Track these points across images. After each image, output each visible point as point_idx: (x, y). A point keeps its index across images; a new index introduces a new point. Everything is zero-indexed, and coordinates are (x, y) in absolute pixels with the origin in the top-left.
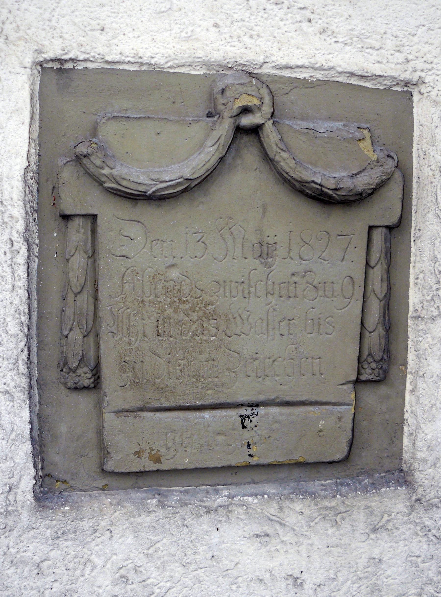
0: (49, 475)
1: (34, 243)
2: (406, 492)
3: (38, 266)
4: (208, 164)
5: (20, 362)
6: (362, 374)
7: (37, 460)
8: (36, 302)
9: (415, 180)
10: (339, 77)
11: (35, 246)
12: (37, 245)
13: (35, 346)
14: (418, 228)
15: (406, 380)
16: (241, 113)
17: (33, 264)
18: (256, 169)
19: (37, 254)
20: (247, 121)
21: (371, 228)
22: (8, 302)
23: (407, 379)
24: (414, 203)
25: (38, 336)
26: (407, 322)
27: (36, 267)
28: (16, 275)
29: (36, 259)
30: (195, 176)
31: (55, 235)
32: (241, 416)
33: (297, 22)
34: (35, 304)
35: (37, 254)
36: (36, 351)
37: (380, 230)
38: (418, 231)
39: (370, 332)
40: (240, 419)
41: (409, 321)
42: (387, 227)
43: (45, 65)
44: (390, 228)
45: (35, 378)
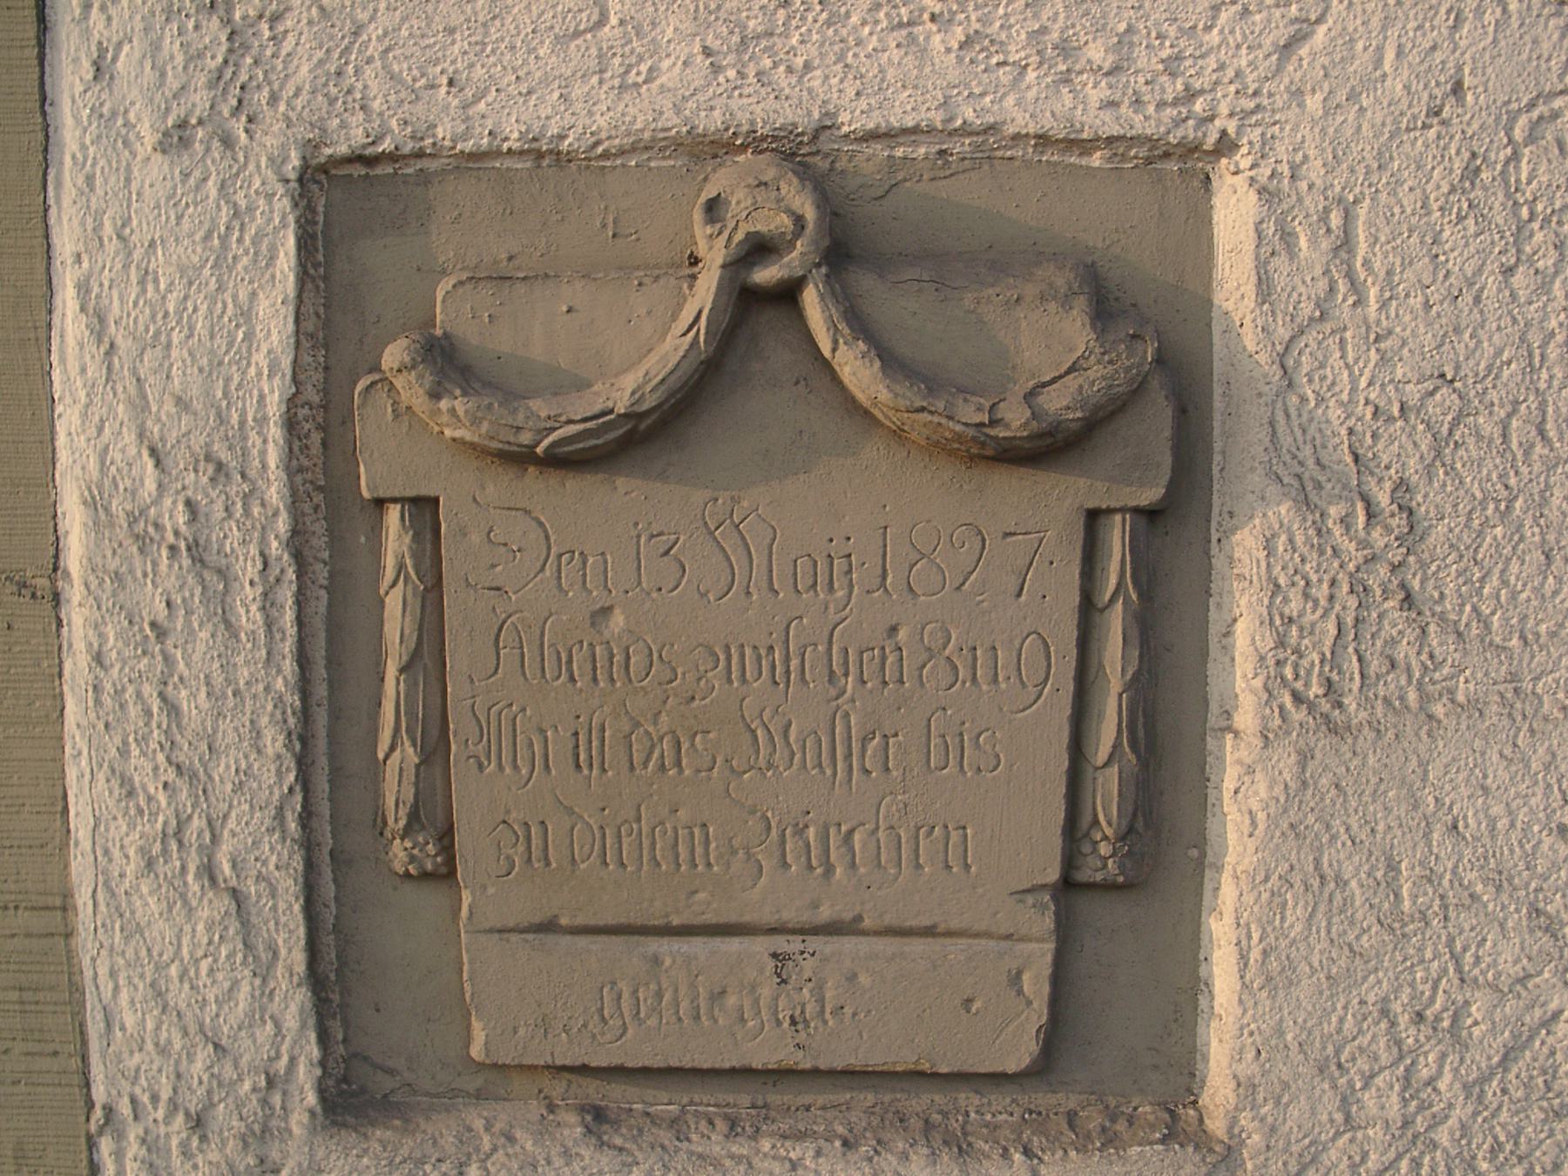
0: (355, 1055)
1: (315, 558)
2: (1198, 1158)
3: (330, 605)
4: (673, 378)
5: (289, 816)
6: (1078, 868)
7: (330, 1023)
8: (325, 685)
9: (1218, 391)
10: (1011, 148)
11: (319, 567)
12: (326, 564)
13: (325, 778)
14: (1226, 509)
15: (1202, 884)
16: (749, 254)
17: (313, 603)
18: (797, 383)
19: (325, 583)
20: (766, 274)
21: (1094, 517)
22: (261, 687)
23: (1206, 880)
24: (1217, 446)
25: (332, 757)
26: (1204, 740)
27: (323, 610)
28: (274, 629)
29: (323, 593)
30: (645, 407)
31: (363, 539)
32: (775, 955)
33: (901, 25)
34: (321, 691)
35: (325, 583)
36: (327, 789)
37: (1118, 518)
38: (1226, 516)
39: (1097, 768)
40: (771, 964)
41: (1209, 739)
42: (1137, 511)
43: (333, 172)
44: (1151, 515)
45: (326, 851)
